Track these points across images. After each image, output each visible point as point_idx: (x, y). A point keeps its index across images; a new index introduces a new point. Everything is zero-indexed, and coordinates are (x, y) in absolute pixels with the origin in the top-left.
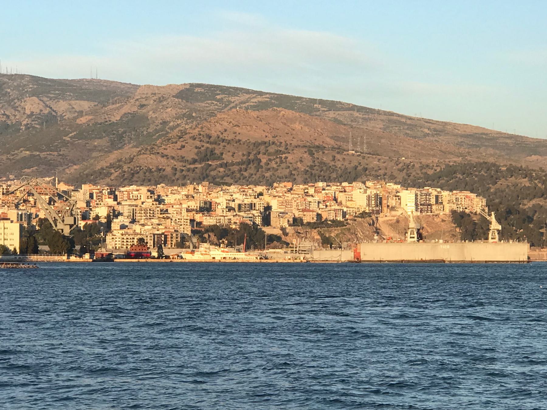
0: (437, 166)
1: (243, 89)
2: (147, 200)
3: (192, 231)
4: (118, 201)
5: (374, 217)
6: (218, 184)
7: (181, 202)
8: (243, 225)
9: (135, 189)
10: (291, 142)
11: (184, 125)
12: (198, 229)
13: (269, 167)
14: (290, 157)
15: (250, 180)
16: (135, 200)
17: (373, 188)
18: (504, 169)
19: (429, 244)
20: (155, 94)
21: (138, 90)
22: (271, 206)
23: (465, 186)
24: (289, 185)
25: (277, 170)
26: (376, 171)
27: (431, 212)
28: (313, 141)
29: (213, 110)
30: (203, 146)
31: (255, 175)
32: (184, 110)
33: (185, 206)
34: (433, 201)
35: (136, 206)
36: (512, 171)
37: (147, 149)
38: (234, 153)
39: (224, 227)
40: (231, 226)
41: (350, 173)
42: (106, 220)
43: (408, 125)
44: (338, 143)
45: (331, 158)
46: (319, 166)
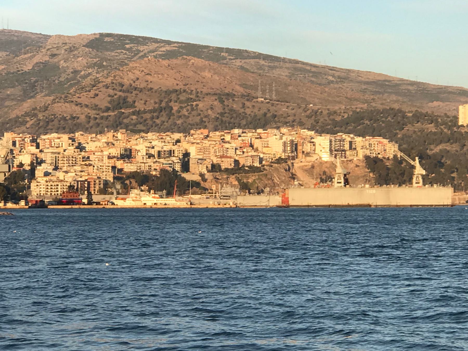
0: (344, 113)
1: (152, 38)
2: (69, 148)
3: (114, 178)
4: (40, 149)
5: (289, 163)
6: (136, 132)
7: (102, 150)
8: (163, 171)
9: (56, 137)
10: (202, 90)
11: (95, 74)
12: (120, 175)
13: (180, 114)
14: (201, 105)
15: (162, 127)
16: (57, 147)
18: (410, 115)
19: (356, 189)
20: (66, 44)
21: (49, 40)
22: (189, 153)
23: (373, 132)
24: (206, 132)
25: (189, 117)
26: (285, 118)
27: (345, 158)
28: (223, 89)
29: (123, 59)
30: (116, 94)
31: (167, 122)
32: (94, 60)
33: (106, 153)
34: (347, 147)
35: (59, 153)
36: (418, 117)
37: (61, 97)
38: (146, 101)
39: (145, 173)
40: (151, 173)
41: (259, 120)
42: (29, 168)
43: (313, 72)
44: (248, 91)
45: (241, 105)
46: (229, 113)
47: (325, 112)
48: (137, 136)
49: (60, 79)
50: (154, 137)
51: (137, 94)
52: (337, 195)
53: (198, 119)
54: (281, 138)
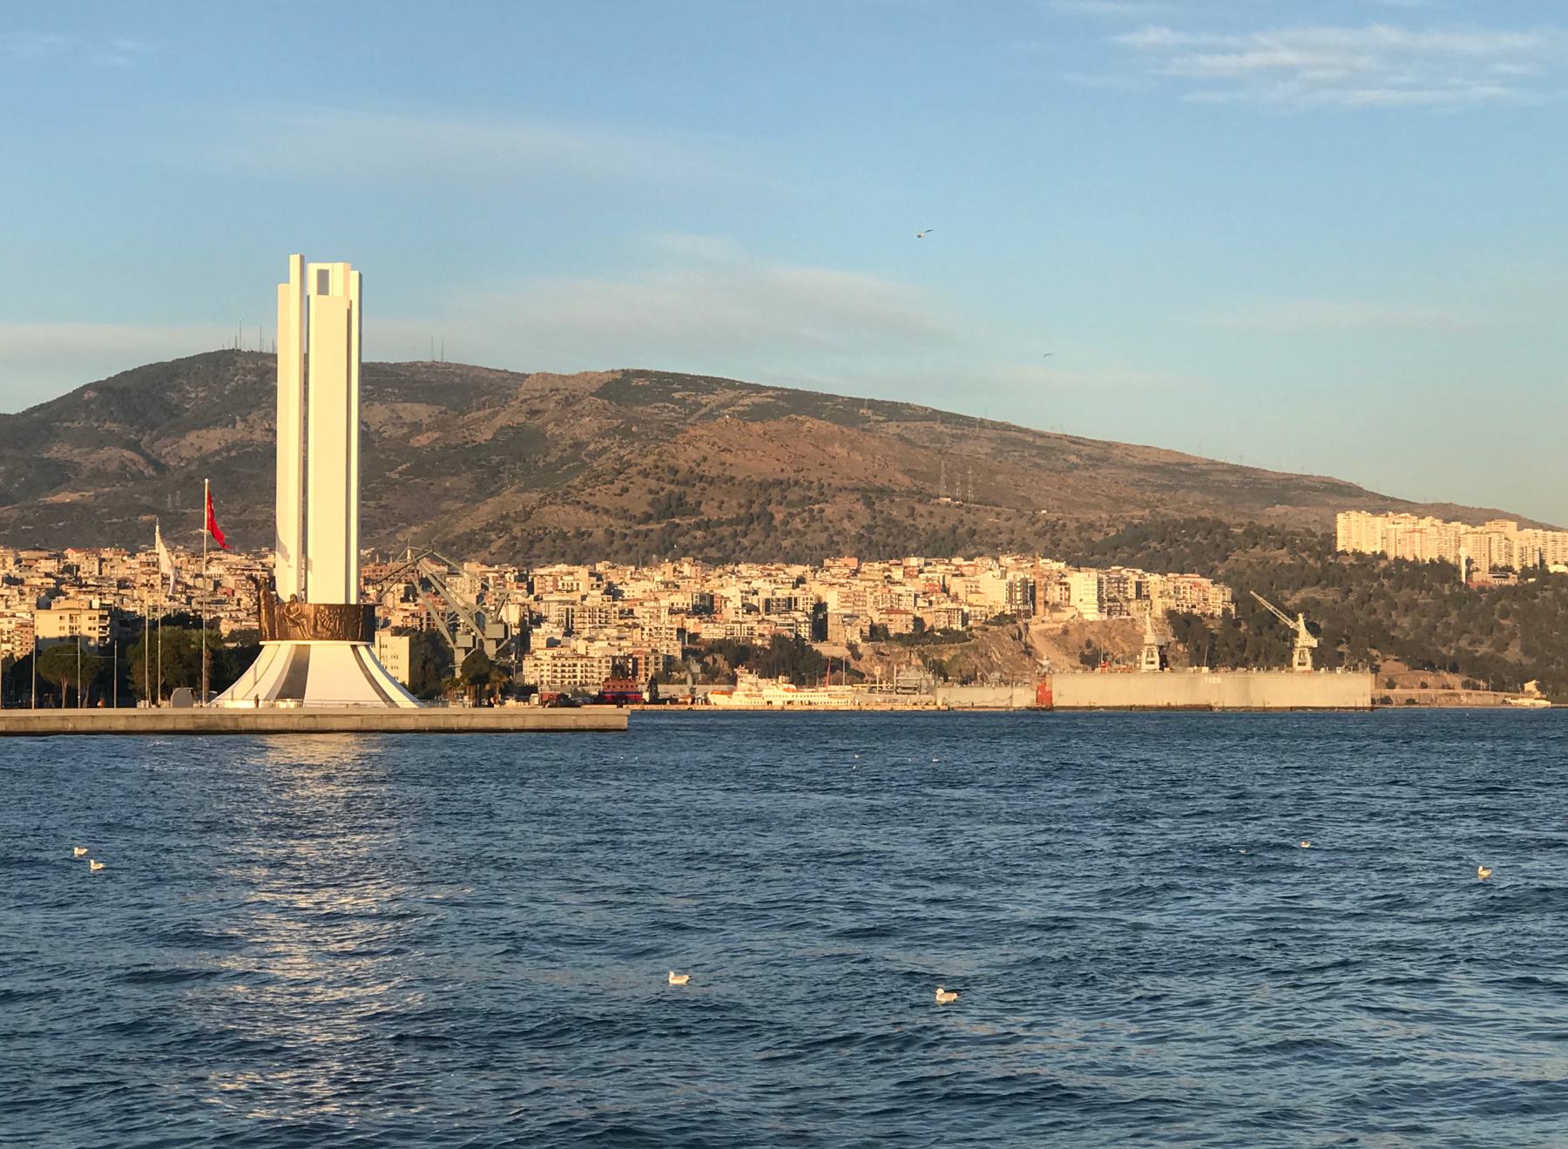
3: (685, 652)
5: (1020, 623)
8: (777, 639)
14: (829, 510)
17: (1016, 569)
33: (665, 603)
34: (1132, 592)
35: (573, 603)
36: (1255, 535)
44: (919, 483)
47: (1071, 526)
48: (719, 571)
49: (549, 459)
50: (755, 573)
51: (704, 489)
52: (1145, 687)
53: (823, 538)
54: (1004, 575)
